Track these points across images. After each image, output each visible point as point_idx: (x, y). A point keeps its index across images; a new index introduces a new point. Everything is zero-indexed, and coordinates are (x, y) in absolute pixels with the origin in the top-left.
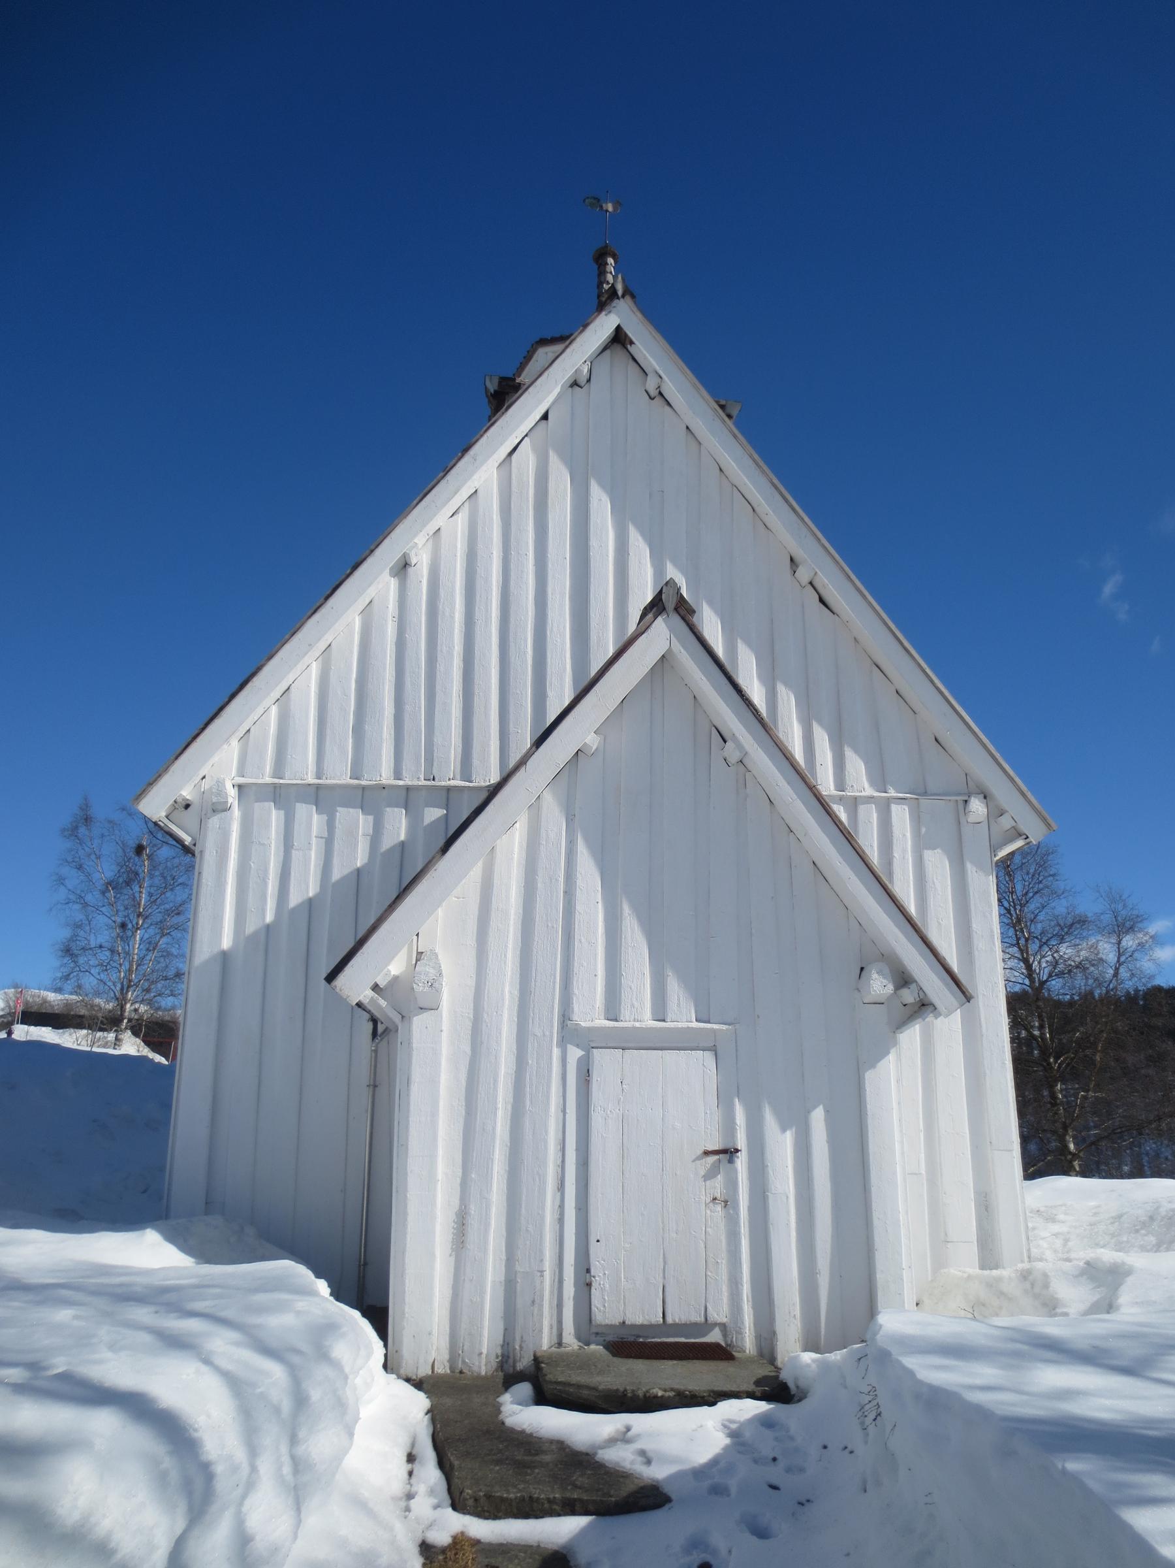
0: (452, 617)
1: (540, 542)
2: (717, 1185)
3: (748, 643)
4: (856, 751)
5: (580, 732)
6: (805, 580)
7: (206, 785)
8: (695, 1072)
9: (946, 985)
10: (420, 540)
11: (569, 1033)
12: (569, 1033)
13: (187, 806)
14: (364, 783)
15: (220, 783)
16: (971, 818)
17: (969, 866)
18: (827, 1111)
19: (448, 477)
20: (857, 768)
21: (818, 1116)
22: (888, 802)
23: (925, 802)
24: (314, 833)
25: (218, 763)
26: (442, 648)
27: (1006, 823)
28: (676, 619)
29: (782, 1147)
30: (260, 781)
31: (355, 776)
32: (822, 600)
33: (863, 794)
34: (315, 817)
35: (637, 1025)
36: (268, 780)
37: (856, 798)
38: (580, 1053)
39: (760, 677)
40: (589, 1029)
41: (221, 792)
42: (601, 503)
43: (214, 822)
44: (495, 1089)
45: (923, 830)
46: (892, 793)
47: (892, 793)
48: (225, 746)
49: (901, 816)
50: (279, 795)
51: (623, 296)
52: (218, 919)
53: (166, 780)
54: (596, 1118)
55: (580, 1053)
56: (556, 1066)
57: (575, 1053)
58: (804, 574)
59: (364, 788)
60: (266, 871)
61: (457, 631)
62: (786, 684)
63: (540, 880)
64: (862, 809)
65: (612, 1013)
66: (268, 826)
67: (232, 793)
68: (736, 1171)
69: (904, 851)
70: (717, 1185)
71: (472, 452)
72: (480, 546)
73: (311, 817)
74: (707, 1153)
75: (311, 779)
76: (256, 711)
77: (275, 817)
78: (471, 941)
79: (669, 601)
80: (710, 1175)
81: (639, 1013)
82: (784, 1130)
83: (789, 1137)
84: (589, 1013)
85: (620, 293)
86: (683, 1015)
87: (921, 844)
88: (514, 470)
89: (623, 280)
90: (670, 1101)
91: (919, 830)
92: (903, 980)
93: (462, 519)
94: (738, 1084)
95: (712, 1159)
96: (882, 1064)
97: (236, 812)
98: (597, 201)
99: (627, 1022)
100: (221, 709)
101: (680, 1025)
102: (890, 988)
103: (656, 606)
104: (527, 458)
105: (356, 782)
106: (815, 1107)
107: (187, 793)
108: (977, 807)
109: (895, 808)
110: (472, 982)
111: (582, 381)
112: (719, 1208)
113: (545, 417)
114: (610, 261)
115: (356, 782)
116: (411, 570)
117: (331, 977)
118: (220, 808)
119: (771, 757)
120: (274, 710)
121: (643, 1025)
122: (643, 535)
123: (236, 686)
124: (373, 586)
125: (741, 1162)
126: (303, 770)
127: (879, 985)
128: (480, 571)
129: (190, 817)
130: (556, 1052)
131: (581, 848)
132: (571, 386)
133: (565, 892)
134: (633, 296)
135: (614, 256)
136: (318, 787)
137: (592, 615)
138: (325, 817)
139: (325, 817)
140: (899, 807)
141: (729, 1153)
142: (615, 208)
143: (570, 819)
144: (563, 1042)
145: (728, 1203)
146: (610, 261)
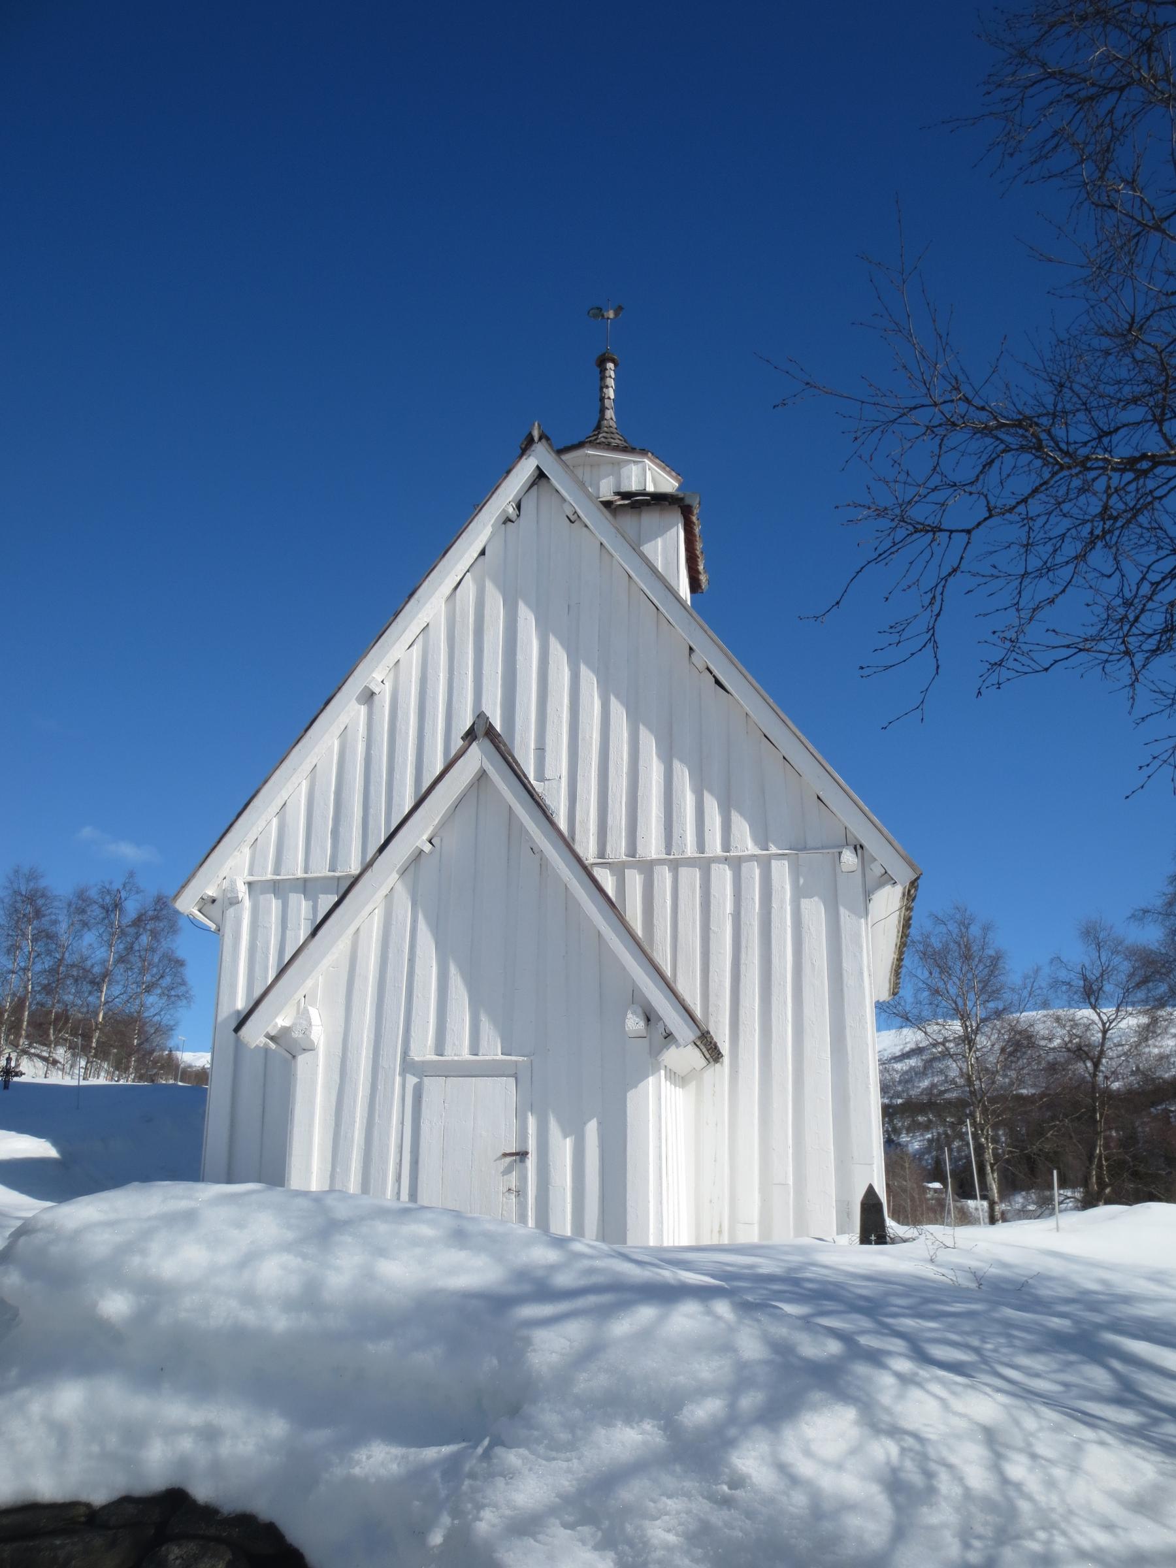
0: (407, 733)
1: (515, 650)
2: (513, 1180)
3: (650, 728)
4: (742, 814)
5: (416, 836)
6: (701, 667)
7: (225, 884)
8: (501, 1094)
9: (685, 1021)
10: (378, 676)
11: (408, 1066)
12: (408, 1066)
13: (214, 901)
14: (337, 874)
15: (233, 883)
16: (845, 868)
17: (842, 910)
18: (599, 1123)
19: (399, 619)
20: (742, 830)
21: (592, 1128)
22: (770, 858)
23: (802, 855)
24: (303, 916)
25: (233, 867)
26: (398, 759)
27: (877, 871)
28: (487, 743)
29: (563, 1149)
30: (264, 878)
31: (332, 870)
32: (718, 682)
33: (746, 853)
34: (304, 902)
35: (456, 1058)
36: (269, 877)
37: (740, 857)
38: (416, 1080)
39: (659, 756)
40: (423, 1062)
41: (233, 888)
42: (527, 619)
43: (231, 912)
44: (355, 1107)
45: (802, 881)
46: (774, 850)
47: (774, 850)
48: (236, 853)
49: (781, 871)
50: (277, 888)
51: (540, 439)
52: (233, 986)
53: (194, 883)
54: (425, 1127)
55: (416, 1080)
56: (397, 1087)
57: (412, 1080)
58: (700, 658)
59: (339, 878)
60: (268, 948)
61: (410, 744)
62: (681, 760)
63: (390, 950)
64: (745, 867)
65: (439, 1049)
66: (269, 912)
67: (242, 891)
68: (526, 1168)
69: (783, 901)
70: (513, 1180)
71: (416, 596)
72: (430, 671)
73: (300, 905)
74: (505, 1155)
75: (300, 874)
76: (260, 822)
77: (275, 904)
78: (342, 1000)
79: (480, 731)
80: (507, 1171)
81: (460, 1050)
82: (565, 1137)
83: (569, 1143)
84: (423, 1051)
85: (536, 438)
86: (493, 1050)
87: (799, 894)
88: (458, 602)
89: (539, 426)
90: (488, 1112)
91: (798, 881)
92: (649, 1017)
93: (416, 650)
94: (535, 1098)
95: (509, 1159)
96: (641, 1085)
97: (247, 903)
98: (599, 312)
99: (450, 1056)
100: (231, 826)
101: (487, 1058)
102: (642, 1024)
103: (470, 736)
104: (469, 585)
105: (332, 874)
106: (589, 1120)
107: (211, 892)
108: (849, 858)
109: (774, 863)
110: (341, 1030)
111: (514, 517)
112: (513, 1196)
113: (483, 553)
114: (610, 365)
115: (332, 874)
116: (376, 698)
117: (237, 1029)
118: (235, 902)
119: (555, 846)
120: (275, 821)
121: (460, 1058)
122: (562, 644)
123: (241, 807)
124: (345, 715)
125: (531, 1162)
126: (295, 869)
127: (634, 1023)
128: (430, 692)
129: (215, 910)
130: (398, 1079)
131: (422, 925)
132: (504, 523)
133: (409, 960)
134: (548, 439)
135: (613, 361)
136: (305, 880)
137: (517, 719)
138: (311, 903)
139: (311, 903)
140: (779, 862)
141: (522, 1155)
142: (616, 314)
143: (414, 904)
144: (403, 1073)
145: (520, 1193)
146: (610, 365)
